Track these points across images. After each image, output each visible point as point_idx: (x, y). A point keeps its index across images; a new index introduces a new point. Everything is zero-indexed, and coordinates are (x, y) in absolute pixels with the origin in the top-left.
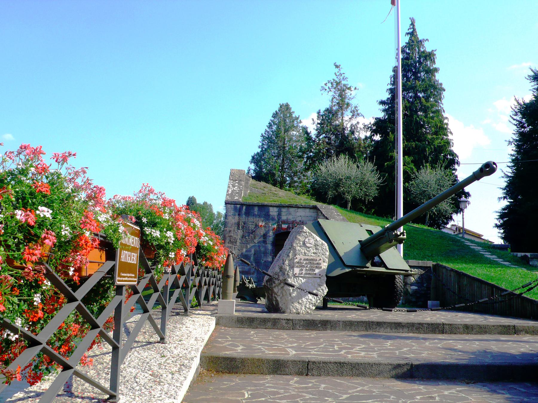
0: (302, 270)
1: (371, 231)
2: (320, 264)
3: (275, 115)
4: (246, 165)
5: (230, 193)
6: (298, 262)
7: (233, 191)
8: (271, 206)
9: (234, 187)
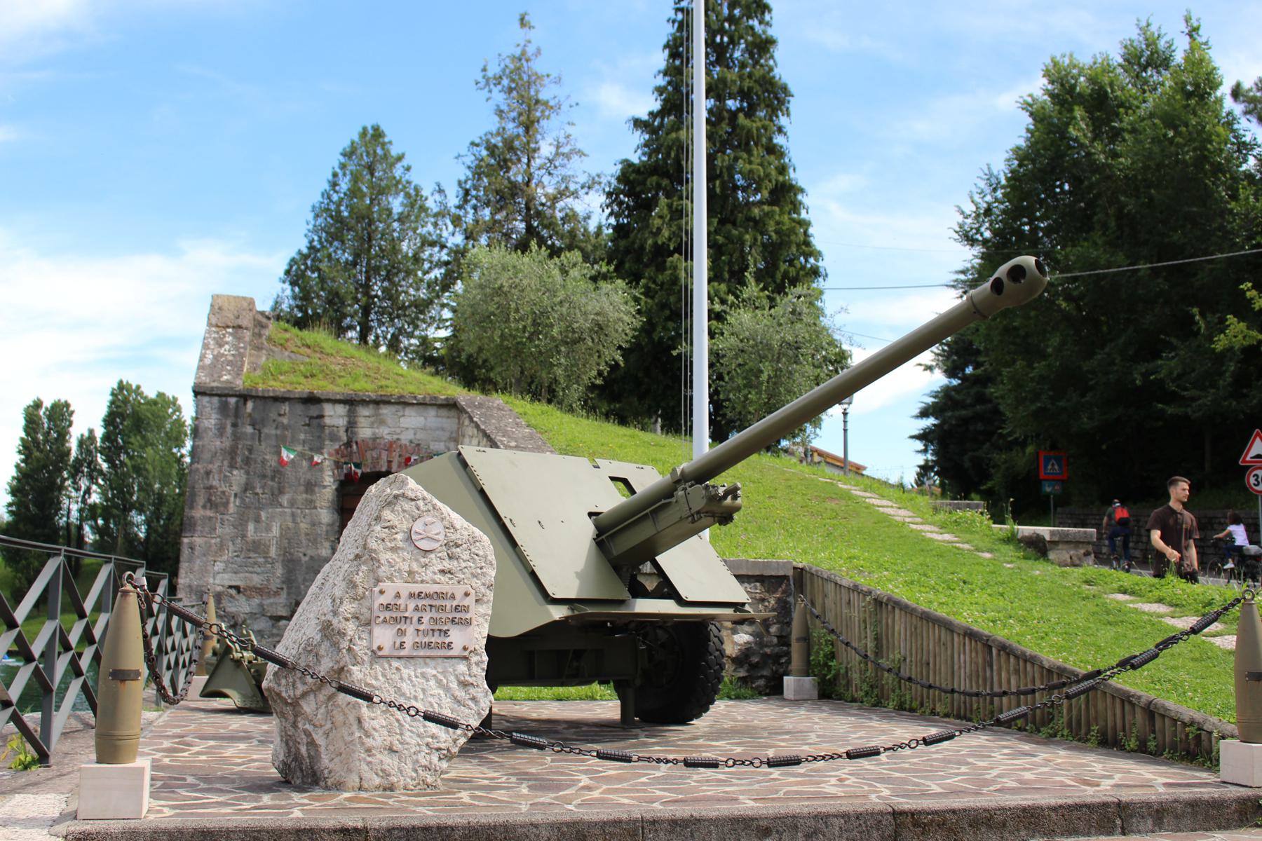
0: (401, 633)
1: (625, 481)
2: (466, 609)
3: (349, 154)
4: (268, 288)
5: (208, 362)
6: (387, 607)
7: (216, 358)
8: (328, 401)
9: (221, 346)
